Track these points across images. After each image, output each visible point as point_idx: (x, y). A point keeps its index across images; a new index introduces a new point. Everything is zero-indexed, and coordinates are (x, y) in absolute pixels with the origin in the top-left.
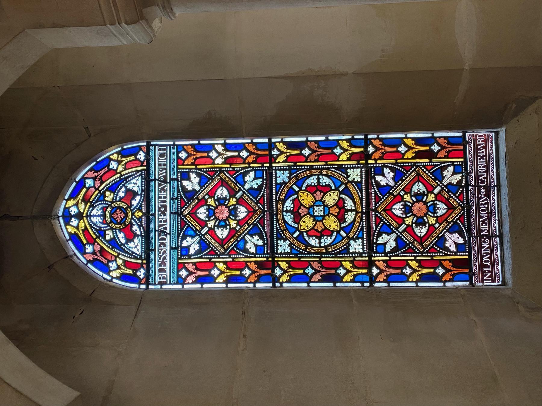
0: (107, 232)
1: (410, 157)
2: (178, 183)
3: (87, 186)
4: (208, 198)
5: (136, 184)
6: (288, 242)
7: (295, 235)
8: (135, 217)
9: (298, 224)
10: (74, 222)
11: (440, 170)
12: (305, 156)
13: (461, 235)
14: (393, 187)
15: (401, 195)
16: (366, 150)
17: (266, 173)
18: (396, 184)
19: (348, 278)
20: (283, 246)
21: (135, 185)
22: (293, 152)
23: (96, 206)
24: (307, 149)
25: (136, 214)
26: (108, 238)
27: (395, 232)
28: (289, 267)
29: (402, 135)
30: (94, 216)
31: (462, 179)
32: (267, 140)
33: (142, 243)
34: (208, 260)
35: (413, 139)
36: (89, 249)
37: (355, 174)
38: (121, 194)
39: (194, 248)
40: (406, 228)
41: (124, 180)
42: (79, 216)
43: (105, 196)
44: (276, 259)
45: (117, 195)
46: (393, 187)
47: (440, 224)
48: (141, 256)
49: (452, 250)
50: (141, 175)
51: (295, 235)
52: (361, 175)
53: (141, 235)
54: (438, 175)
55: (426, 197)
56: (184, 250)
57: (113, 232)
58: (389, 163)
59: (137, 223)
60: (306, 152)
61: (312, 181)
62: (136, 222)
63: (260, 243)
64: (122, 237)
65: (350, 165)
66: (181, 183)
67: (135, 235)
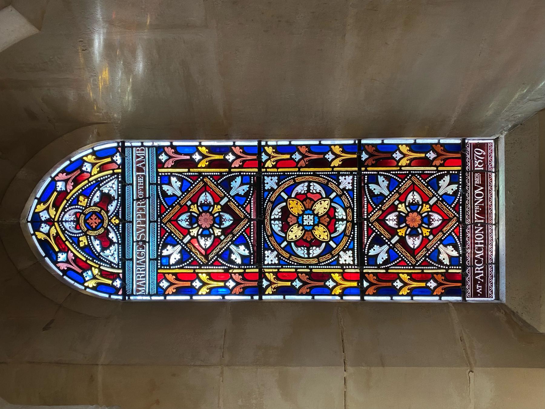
0: (81, 239)
1: (204, 166)
2: (157, 187)
3: (58, 190)
4: (398, 204)
5: (112, 187)
6: (342, 253)
7: (283, 245)
8: (112, 223)
9: (286, 233)
10: (45, 228)
11: (436, 179)
12: (396, 160)
13: (456, 248)
14: (387, 197)
15: (187, 205)
16: (360, 157)
17: (254, 179)
18: (391, 193)
19: (204, 290)
20: (270, 257)
21: (111, 187)
22: (250, 157)
23: (68, 211)
24: (230, 154)
25: (113, 221)
26: (82, 245)
27: (180, 244)
28: (176, 279)
29: (230, 143)
30: (66, 221)
31: (250, 190)
32: (255, 143)
33: (119, 251)
34: (420, 271)
35: (207, 147)
36: (62, 257)
37: (346, 182)
38: (96, 199)
39: (175, 257)
40: (190, 240)
41: (98, 184)
42: (50, 222)
43: (78, 201)
44: (365, 271)
45: (92, 199)
46: (387, 197)
47: (434, 237)
48: (118, 265)
49: (445, 263)
50: (118, 178)
51: (283, 245)
52: (353, 183)
53: (118, 243)
54: (435, 185)
55: (212, 208)
56: (371, 259)
57: (87, 238)
58: (176, 173)
59: (114, 230)
60: (297, 157)
61: (302, 188)
62: (113, 228)
63: (246, 253)
64: (98, 245)
65: (292, 172)
66: (161, 188)
67: (112, 243)
